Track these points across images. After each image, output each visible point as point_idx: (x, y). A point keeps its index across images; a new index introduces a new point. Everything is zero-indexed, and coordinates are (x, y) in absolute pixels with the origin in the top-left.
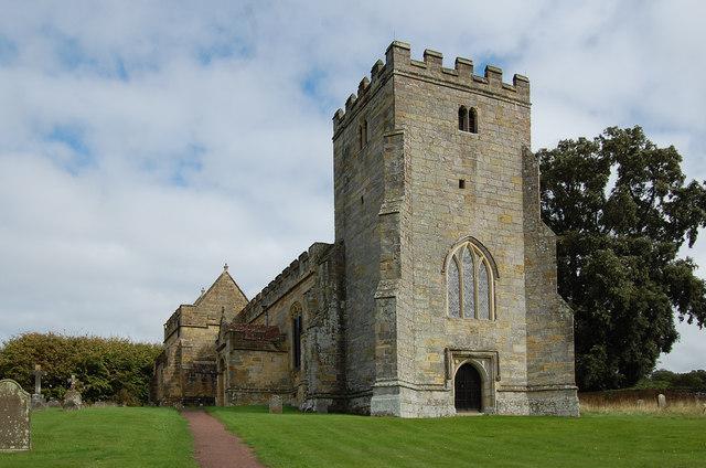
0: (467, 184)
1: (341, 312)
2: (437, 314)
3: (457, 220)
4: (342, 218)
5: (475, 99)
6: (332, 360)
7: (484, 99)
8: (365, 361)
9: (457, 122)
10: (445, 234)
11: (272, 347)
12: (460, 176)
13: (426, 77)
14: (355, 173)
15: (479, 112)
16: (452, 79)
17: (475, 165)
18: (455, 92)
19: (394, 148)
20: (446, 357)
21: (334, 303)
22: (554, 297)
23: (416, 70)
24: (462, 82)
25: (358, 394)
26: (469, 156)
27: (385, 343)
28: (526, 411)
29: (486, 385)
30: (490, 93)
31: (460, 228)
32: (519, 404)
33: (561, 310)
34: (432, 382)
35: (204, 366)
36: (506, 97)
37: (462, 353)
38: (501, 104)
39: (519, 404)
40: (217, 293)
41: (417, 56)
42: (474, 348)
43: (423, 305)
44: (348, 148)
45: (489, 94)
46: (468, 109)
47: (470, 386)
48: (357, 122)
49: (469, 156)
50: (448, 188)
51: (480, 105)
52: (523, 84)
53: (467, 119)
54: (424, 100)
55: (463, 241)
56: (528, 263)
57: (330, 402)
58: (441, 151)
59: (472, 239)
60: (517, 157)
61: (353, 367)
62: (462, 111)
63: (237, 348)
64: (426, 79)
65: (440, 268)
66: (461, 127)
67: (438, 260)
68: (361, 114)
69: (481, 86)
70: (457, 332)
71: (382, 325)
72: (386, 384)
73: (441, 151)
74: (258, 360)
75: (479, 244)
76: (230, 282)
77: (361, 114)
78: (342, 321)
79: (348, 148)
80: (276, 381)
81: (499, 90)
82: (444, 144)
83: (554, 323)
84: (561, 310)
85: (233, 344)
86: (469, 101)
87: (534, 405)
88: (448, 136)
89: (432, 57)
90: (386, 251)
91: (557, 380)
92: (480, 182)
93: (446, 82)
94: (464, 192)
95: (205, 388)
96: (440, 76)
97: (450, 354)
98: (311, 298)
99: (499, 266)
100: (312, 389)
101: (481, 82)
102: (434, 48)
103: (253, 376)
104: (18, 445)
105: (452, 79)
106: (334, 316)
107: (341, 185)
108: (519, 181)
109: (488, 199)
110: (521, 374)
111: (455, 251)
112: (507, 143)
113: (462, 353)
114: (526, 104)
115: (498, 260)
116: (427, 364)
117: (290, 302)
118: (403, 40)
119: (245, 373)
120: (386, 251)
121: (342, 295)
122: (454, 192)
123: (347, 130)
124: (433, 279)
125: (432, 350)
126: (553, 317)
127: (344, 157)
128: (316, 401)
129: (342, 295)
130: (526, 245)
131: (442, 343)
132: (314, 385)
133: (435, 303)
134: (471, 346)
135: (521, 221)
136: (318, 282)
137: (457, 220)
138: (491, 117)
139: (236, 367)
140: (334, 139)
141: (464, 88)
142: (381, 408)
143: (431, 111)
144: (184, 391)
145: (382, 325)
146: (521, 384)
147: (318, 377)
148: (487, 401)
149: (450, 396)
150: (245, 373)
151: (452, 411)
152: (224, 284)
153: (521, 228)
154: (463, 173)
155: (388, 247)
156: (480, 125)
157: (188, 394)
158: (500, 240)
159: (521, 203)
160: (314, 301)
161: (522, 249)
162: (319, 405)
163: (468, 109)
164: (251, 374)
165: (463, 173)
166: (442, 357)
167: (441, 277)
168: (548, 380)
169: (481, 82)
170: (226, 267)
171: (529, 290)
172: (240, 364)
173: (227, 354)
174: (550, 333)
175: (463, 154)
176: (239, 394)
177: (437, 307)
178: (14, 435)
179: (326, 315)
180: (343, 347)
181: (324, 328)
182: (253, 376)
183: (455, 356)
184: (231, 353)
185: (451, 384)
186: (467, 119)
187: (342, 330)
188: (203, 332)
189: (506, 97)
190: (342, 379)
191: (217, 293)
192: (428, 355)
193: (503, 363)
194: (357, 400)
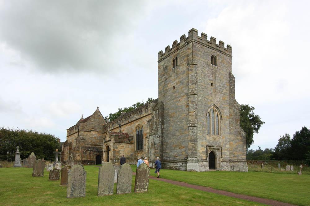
0: (213, 85)
1: (162, 130)
3: (210, 98)
4: (162, 91)
5: (216, 53)
6: (159, 148)
7: (218, 53)
8: (174, 149)
10: (207, 103)
11: (128, 141)
12: (211, 82)
14: (171, 76)
15: (217, 58)
16: (218, 48)
17: (216, 78)
20: (207, 149)
21: (160, 126)
22: (239, 128)
23: (200, 40)
24: (213, 46)
25: (170, 162)
26: (214, 74)
29: (217, 160)
30: (221, 51)
32: (227, 167)
33: (242, 133)
35: (89, 148)
36: (225, 53)
37: (212, 147)
38: (224, 56)
39: (227, 167)
40: (94, 118)
42: (215, 145)
44: (167, 67)
45: (220, 51)
46: (214, 56)
48: (172, 57)
49: (214, 74)
50: (208, 86)
52: (230, 48)
53: (213, 59)
54: (201, 52)
56: (231, 115)
58: (206, 72)
59: (215, 105)
60: (228, 76)
61: (167, 151)
62: (212, 57)
63: (116, 142)
64: (202, 44)
65: (205, 116)
67: (205, 112)
68: (175, 54)
69: (218, 48)
72: (193, 159)
73: (206, 72)
74: (123, 147)
75: (217, 107)
77: (175, 54)
78: (162, 133)
80: (129, 155)
81: (223, 50)
82: (207, 69)
83: (239, 137)
84: (242, 133)
85: (115, 140)
86: (215, 53)
87: (233, 167)
89: (221, 43)
90: (191, 109)
91: (240, 158)
92: (217, 84)
93: (208, 46)
95: (90, 157)
96: (206, 43)
97: (208, 148)
98: (151, 124)
101: (218, 47)
102: (205, 32)
104: (144, 189)
106: (160, 131)
107: (162, 80)
108: (228, 85)
109: (219, 91)
110: (228, 156)
115: (222, 113)
116: (201, 151)
117: (138, 123)
119: (119, 152)
120: (191, 109)
121: (163, 124)
122: (209, 87)
123: (166, 59)
125: (202, 146)
126: (239, 135)
127: (164, 70)
129: (163, 124)
130: (230, 108)
133: (203, 129)
135: (228, 99)
136: (153, 117)
138: (221, 61)
140: (159, 62)
141: (213, 48)
142: (191, 168)
144: (82, 158)
145: (191, 137)
147: (154, 155)
148: (217, 166)
150: (119, 152)
151: (208, 168)
152: (97, 113)
153: (228, 102)
155: (192, 107)
156: (218, 63)
157: (84, 159)
158: (222, 106)
159: (228, 92)
160: (151, 125)
163: (214, 56)
164: (121, 152)
166: (206, 149)
169: (218, 47)
170: (98, 107)
171: (231, 125)
174: (238, 141)
175: (213, 73)
176: (116, 160)
177: (204, 130)
178: (144, 185)
179: (157, 131)
180: (163, 143)
181: (156, 136)
184: (114, 144)
185: (208, 158)
186: (213, 59)
187: (162, 137)
188: (89, 133)
189: (217, 49)
191: (94, 118)
193: (223, 151)
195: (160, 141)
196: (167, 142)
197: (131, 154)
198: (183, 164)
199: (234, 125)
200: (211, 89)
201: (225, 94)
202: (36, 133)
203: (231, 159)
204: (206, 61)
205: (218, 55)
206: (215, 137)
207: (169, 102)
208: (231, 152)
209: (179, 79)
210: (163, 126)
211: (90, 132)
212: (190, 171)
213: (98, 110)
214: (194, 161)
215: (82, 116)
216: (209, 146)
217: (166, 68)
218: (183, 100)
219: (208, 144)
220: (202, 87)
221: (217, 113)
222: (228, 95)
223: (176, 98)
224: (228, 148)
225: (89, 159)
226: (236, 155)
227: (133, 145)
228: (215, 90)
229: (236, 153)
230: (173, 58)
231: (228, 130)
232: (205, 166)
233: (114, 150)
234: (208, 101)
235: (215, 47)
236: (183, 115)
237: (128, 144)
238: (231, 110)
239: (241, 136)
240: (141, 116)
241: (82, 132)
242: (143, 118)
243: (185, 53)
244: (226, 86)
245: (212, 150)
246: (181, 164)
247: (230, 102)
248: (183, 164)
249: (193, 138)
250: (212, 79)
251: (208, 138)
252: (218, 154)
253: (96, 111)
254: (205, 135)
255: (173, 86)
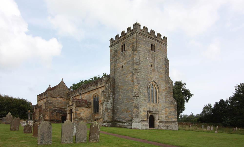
0: (153, 66)
1: (113, 98)
2: (146, 101)
3: (150, 76)
7: (157, 42)
8: (123, 113)
9: (151, 48)
11: (87, 106)
12: (151, 64)
13: (144, 34)
14: (120, 58)
15: (156, 46)
16: (150, 36)
18: (151, 39)
19: (137, 54)
20: (147, 113)
21: (112, 95)
22: (172, 99)
23: (142, 32)
24: (152, 37)
26: (153, 58)
27: (136, 109)
28: (165, 128)
29: (156, 121)
30: (159, 41)
31: (151, 78)
32: (163, 126)
34: (144, 120)
36: (162, 42)
37: (151, 112)
39: (163, 126)
40: (60, 87)
41: (142, 28)
43: (142, 99)
45: (158, 41)
46: (153, 45)
47: (152, 121)
49: (153, 58)
51: (156, 44)
52: (166, 39)
53: (153, 47)
54: (143, 41)
55: (152, 82)
56: (166, 89)
57: (111, 124)
58: (147, 56)
59: (154, 81)
62: (152, 45)
63: (77, 106)
66: (152, 50)
67: (146, 86)
68: (123, 41)
69: (157, 39)
70: (150, 106)
71: (135, 104)
73: (147, 56)
74: (83, 110)
75: (155, 83)
76: (64, 84)
78: (114, 101)
79: (116, 51)
80: (88, 116)
82: (148, 54)
83: (172, 105)
86: (155, 42)
87: (167, 127)
88: (149, 52)
89: (159, 35)
91: (173, 120)
92: (156, 65)
93: (149, 36)
94: (152, 68)
95: (57, 117)
96: (147, 34)
98: (104, 93)
99: (159, 89)
100: (106, 120)
101: (157, 37)
103: (82, 115)
105: (150, 36)
106: (112, 99)
108: (164, 66)
109: (157, 70)
110: (164, 118)
111: (149, 84)
112: (162, 55)
113: (151, 112)
114: (166, 45)
116: (143, 115)
118: (139, 22)
119: (79, 114)
121: (114, 93)
122: (150, 67)
124: (145, 92)
125: (144, 111)
128: (107, 123)
129: (114, 93)
130: (166, 84)
131: (147, 109)
132: (106, 119)
133: (145, 98)
134: (153, 110)
136: (106, 89)
137: (150, 76)
139: (77, 112)
140: (110, 46)
141: (153, 39)
142: (135, 127)
143: (145, 44)
144: (50, 118)
146: (163, 121)
147: (107, 116)
148: (156, 125)
149: (147, 124)
150: (79, 114)
151: (148, 127)
152: (62, 84)
153: (164, 79)
154: (152, 63)
155: (136, 82)
157: (52, 119)
158: (160, 82)
160: (105, 94)
161: (164, 85)
162: (108, 124)
163: (153, 45)
164: (81, 114)
165: (152, 63)
167: (146, 91)
168: (170, 120)
169: (157, 37)
170: (62, 79)
172: (78, 111)
173: (74, 108)
175: (152, 57)
176: (78, 120)
177: (146, 99)
178: (96, 137)
181: (109, 102)
182: (82, 115)
183: (149, 113)
184: (76, 108)
186: (153, 47)
187: (114, 103)
188: (55, 99)
189: (162, 42)
190: (113, 117)
192: (143, 112)
193: (160, 115)
194: (119, 124)
195: (112, 107)
196: (117, 108)
197: (90, 115)
198: (129, 124)
199: (168, 96)
200: (151, 69)
201: (162, 73)
202: (11, 97)
203: (166, 121)
204: (147, 48)
205: (156, 44)
206: (154, 104)
207: (118, 78)
208: (166, 116)
209: (126, 60)
210: (114, 95)
211: (57, 98)
212: (135, 129)
213: (63, 81)
214: (137, 122)
215: (50, 86)
216: (149, 111)
217: (116, 52)
218: (129, 76)
219: (148, 109)
220: (144, 67)
221: (155, 87)
222: (164, 74)
223: (124, 74)
224: (164, 113)
225: (56, 119)
226: (170, 118)
227: (91, 109)
228: (154, 70)
229: (170, 116)
230: (122, 44)
231: (164, 100)
232: (146, 126)
233: (75, 112)
234: (149, 78)
235: (154, 38)
236: (129, 88)
237: (87, 108)
238: (167, 85)
239: (173, 105)
240: (97, 87)
241: (50, 98)
242: (98, 89)
243: (131, 41)
244: (162, 67)
245: (152, 114)
246: (128, 124)
247: (165, 79)
248: (129, 124)
249: (136, 105)
250: (152, 61)
251: (148, 105)
252: (156, 117)
253: (61, 82)
254: (146, 103)
255: (121, 66)
